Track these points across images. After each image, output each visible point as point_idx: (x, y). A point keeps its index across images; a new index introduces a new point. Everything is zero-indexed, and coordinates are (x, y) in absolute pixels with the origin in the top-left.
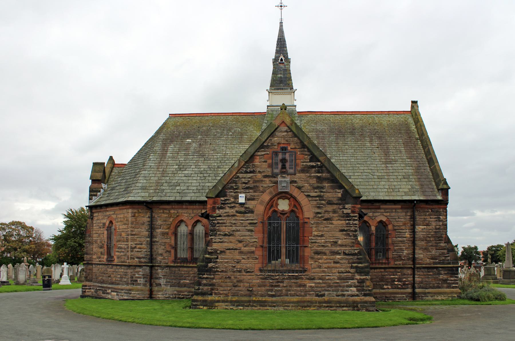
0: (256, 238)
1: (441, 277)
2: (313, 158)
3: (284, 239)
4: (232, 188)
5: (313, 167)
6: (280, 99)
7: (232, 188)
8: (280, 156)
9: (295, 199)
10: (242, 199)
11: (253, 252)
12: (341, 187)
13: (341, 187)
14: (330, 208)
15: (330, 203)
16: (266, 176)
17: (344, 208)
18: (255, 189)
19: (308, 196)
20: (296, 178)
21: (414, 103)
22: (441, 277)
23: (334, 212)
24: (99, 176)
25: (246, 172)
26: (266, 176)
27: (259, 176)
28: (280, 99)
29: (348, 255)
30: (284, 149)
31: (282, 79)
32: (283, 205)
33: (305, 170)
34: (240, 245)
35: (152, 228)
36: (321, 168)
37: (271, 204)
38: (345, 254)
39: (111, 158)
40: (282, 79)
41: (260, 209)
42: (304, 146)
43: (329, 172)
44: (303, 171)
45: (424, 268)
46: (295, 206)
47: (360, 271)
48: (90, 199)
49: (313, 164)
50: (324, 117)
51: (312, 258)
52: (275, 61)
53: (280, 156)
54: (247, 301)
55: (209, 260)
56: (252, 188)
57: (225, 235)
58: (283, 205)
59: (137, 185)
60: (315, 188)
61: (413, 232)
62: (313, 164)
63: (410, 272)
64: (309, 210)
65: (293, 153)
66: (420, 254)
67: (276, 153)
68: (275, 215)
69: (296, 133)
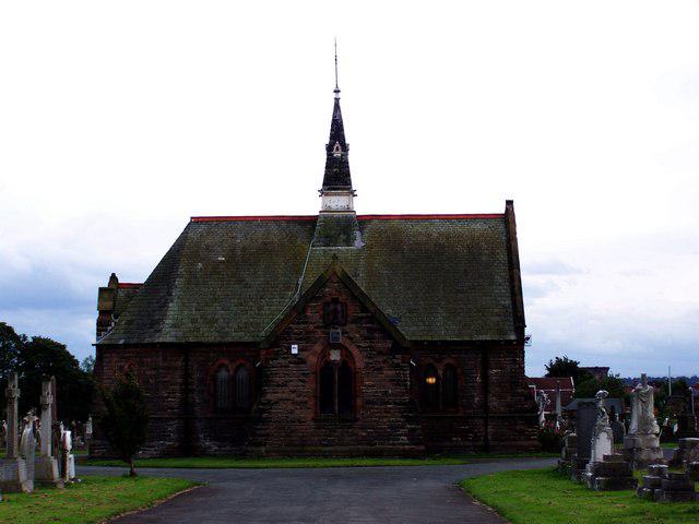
0: (310, 387)
1: (518, 427)
2: (364, 309)
3: (336, 389)
4: (285, 339)
5: (363, 318)
6: (338, 202)
7: (285, 339)
8: (332, 307)
9: (346, 349)
10: (295, 351)
11: (306, 402)
12: (390, 337)
13: (390, 337)
14: (380, 359)
15: (380, 353)
16: (318, 327)
17: (394, 358)
18: (307, 339)
19: (359, 347)
20: (347, 328)
21: (510, 203)
22: (518, 427)
23: (384, 362)
24: (109, 305)
25: (298, 323)
26: (318, 327)
27: (311, 327)
28: (338, 202)
29: (399, 404)
30: (335, 301)
31: (337, 176)
32: (335, 356)
33: (356, 321)
34: (293, 396)
35: (187, 375)
36: (372, 319)
37: (325, 354)
38: (396, 403)
39: (113, 278)
40: (337, 176)
41: (312, 359)
42: (354, 297)
43: (379, 323)
44: (353, 322)
45: (499, 417)
46: (346, 356)
47: (409, 420)
48: (98, 335)
49: (364, 315)
50: (395, 223)
51: (363, 407)
52: (329, 148)
53: (332, 307)
54: (297, 449)
55: (264, 411)
56: (305, 340)
57: (279, 386)
58: (335, 356)
59: (167, 322)
60: (365, 338)
61: (485, 376)
62: (364, 315)
63: (482, 422)
64: (360, 361)
65: (344, 305)
66: (494, 402)
67: (327, 304)
68: (327, 368)
69: (346, 282)
